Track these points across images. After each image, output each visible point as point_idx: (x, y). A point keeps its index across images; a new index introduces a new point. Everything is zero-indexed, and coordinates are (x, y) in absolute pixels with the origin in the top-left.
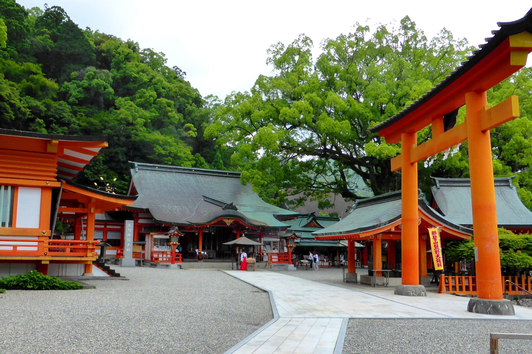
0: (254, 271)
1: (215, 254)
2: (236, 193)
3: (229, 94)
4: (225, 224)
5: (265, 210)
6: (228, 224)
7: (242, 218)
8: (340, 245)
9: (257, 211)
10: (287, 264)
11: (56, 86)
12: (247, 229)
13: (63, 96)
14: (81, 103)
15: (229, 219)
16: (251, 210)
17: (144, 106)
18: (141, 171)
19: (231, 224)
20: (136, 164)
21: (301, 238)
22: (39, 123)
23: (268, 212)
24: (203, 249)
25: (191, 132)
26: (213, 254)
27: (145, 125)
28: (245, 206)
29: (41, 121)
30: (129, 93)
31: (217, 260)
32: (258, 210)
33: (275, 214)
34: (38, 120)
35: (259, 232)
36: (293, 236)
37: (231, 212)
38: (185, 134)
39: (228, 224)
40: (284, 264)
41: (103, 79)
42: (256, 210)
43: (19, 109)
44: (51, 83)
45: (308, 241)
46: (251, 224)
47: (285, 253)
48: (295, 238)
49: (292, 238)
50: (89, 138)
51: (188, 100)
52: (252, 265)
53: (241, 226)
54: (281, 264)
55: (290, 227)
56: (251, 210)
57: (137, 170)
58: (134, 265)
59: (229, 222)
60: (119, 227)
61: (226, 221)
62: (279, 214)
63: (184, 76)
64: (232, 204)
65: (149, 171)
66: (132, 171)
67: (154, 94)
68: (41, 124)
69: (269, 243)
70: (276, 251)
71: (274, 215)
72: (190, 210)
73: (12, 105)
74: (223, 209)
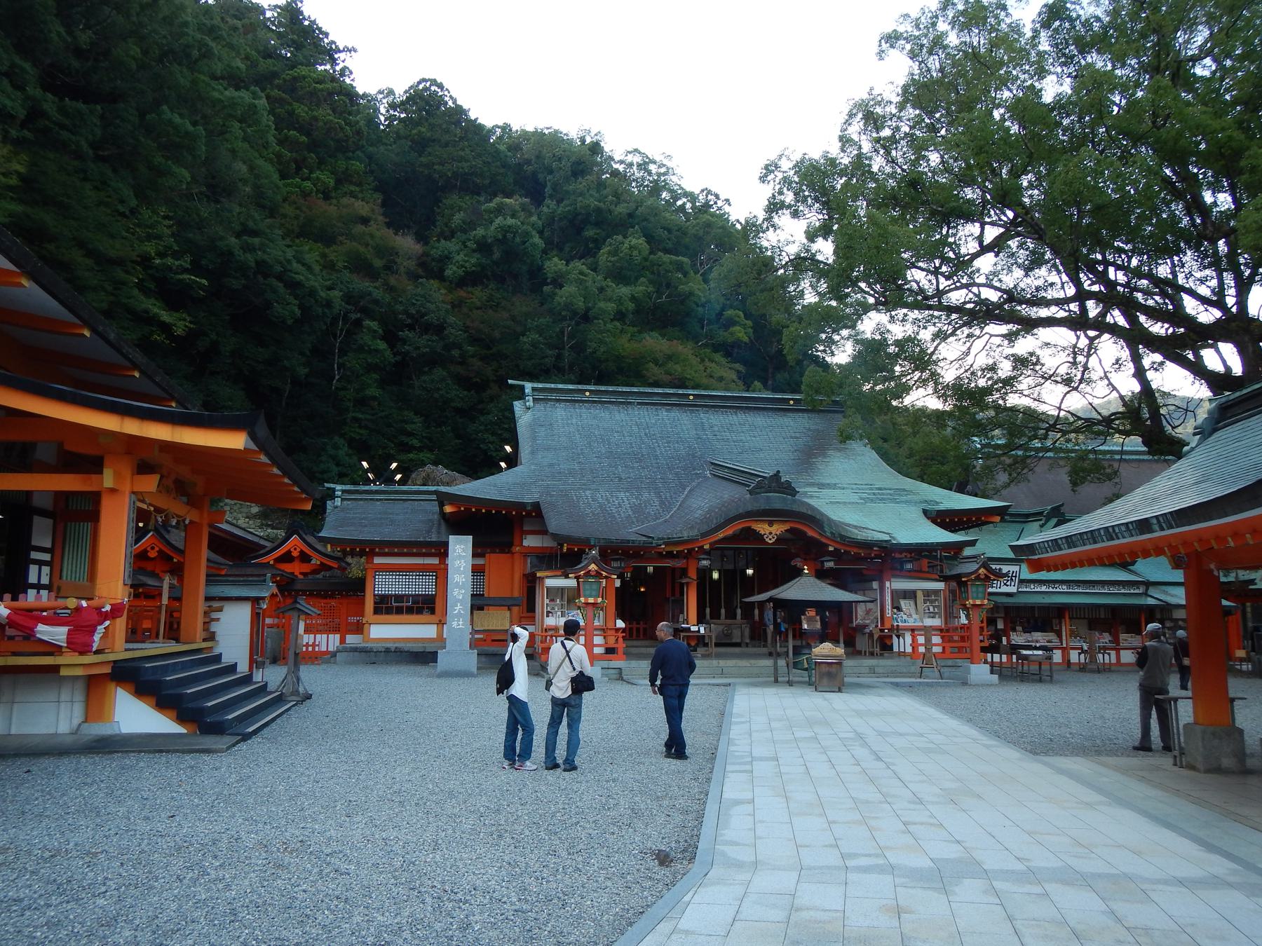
0: (840, 691)
1: (747, 632)
2: (810, 454)
3: (773, 157)
4: (759, 538)
5: (896, 496)
6: (770, 540)
7: (814, 519)
8: (1150, 601)
9: (872, 501)
10: (965, 663)
11: (418, 248)
12: (831, 554)
13: (431, 268)
14: (470, 279)
15: (771, 524)
16: (854, 498)
17: (620, 275)
18: (540, 406)
19: (780, 540)
20: (528, 386)
21: (1021, 581)
22: (369, 328)
23: (906, 502)
24: (700, 621)
25: (737, 328)
26: (740, 630)
27: (620, 316)
28: (833, 486)
29: (373, 325)
30: (588, 251)
31: (751, 650)
32: (880, 496)
33: (929, 507)
34: (367, 322)
35: (866, 562)
36: (982, 571)
37: (776, 500)
38: (722, 335)
39: (770, 540)
40: (960, 662)
41: (510, 214)
42: (865, 499)
43: (312, 293)
44: (407, 244)
45: (1044, 589)
46: (842, 536)
47: (963, 627)
48: (987, 578)
49: (978, 578)
50: (427, 333)
51: (700, 234)
52: (833, 669)
53: (810, 544)
54: (950, 662)
55: (972, 543)
56: (854, 498)
57: (530, 403)
58: (475, 670)
59: (770, 532)
60: (435, 561)
61: (763, 528)
62: (941, 507)
63: (727, 208)
64: (777, 476)
65: (563, 405)
66: (518, 406)
67: (641, 242)
68: (375, 331)
69: (911, 595)
70: (937, 622)
71: (925, 512)
72: (662, 503)
73: (293, 286)
74: (751, 492)
